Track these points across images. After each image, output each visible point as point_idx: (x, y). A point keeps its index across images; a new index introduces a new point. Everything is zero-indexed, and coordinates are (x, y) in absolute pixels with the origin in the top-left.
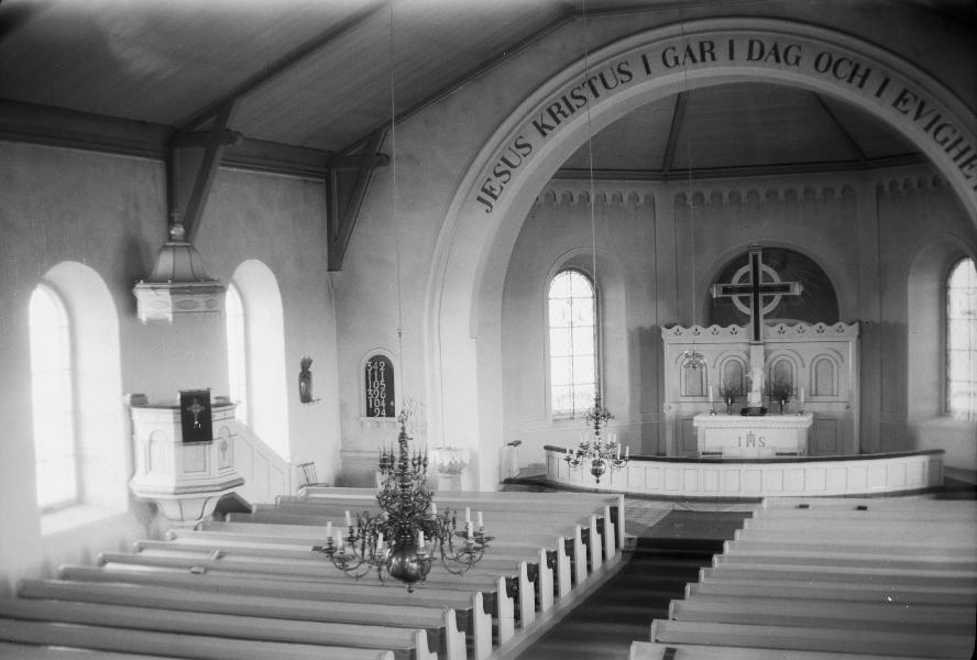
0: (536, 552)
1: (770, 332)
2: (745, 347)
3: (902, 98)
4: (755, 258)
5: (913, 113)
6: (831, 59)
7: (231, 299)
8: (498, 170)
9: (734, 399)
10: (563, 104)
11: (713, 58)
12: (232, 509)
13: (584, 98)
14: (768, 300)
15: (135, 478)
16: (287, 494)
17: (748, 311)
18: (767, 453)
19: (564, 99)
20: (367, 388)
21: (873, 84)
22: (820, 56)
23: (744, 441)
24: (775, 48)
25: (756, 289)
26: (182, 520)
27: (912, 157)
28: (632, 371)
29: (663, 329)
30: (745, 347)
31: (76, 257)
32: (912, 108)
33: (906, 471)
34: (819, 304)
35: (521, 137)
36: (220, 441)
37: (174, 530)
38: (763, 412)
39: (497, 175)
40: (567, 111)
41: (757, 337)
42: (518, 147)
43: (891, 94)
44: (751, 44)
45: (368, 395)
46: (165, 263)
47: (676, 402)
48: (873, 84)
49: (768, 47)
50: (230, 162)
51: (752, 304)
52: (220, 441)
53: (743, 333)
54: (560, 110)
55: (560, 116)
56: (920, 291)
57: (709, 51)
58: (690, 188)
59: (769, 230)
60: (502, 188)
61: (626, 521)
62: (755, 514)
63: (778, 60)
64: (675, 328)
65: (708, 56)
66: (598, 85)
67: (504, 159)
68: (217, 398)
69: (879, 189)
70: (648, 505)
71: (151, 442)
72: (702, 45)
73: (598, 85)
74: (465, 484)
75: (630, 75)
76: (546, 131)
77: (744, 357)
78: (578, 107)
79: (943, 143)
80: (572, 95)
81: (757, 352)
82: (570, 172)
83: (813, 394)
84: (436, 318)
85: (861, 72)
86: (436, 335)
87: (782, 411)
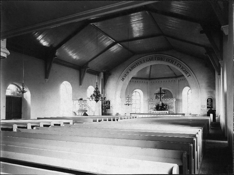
24: (161, 58)
31: (69, 81)
49: (160, 58)
66: (138, 64)
73: (138, 64)
82: (133, 78)
85: (173, 61)
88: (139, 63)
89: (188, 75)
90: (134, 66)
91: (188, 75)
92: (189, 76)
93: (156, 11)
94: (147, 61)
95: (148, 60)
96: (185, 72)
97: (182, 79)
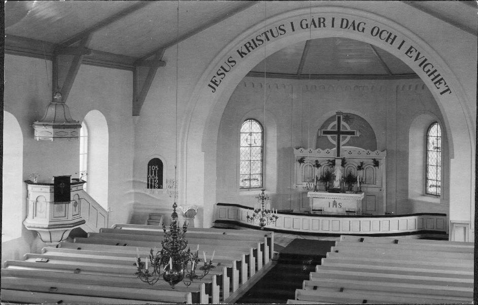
0: (231, 262)
4: (339, 118)
5: (414, 58)
6: (379, 30)
7: (83, 131)
12: (78, 236)
13: (262, 41)
15: (27, 220)
16: (106, 227)
17: (335, 143)
18: (340, 211)
19: (253, 40)
20: (148, 174)
22: (374, 28)
23: (331, 205)
24: (354, 23)
25: (339, 133)
26: (51, 242)
27: (414, 75)
29: (295, 150)
33: (408, 223)
35: (231, 57)
36: (74, 201)
37: (46, 248)
39: (219, 75)
40: (254, 46)
42: (230, 62)
44: (343, 20)
45: (148, 178)
46: (51, 112)
50: (85, 62)
51: (341, 127)
52: (74, 201)
55: (250, 48)
56: (415, 137)
57: (323, 22)
60: (220, 81)
61: (274, 244)
62: (336, 243)
63: (354, 29)
64: (301, 149)
65: (322, 24)
66: (269, 35)
67: (222, 67)
68: (73, 179)
70: (285, 236)
71: (37, 201)
72: (319, 19)
73: (269, 35)
74: (196, 223)
76: (243, 55)
78: (259, 45)
79: (427, 72)
80: (257, 39)
82: (254, 73)
84: (185, 140)
85: (392, 37)
86: (185, 160)
87: (350, 190)
89: (443, 88)
91: (443, 88)
94: (304, 26)
96: (432, 77)
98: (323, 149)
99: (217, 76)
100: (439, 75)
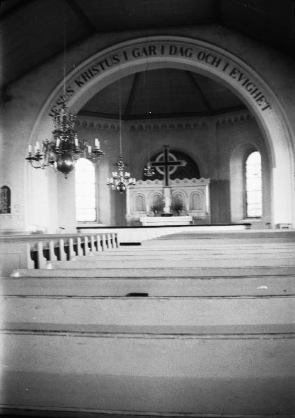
1: (173, 183)
2: (161, 189)
3: (233, 72)
5: (237, 79)
6: (205, 54)
8: (59, 102)
9: (158, 209)
10: (88, 73)
11: (155, 53)
14: (171, 169)
19: (89, 71)
21: (222, 66)
28: (111, 203)
30: (161, 189)
32: (237, 76)
34: (191, 171)
38: (170, 215)
39: (59, 104)
41: (167, 184)
43: (229, 70)
44: (171, 47)
47: (131, 213)
48: (222, 66)
51: (168, 158)
53: (161, 183)
54: (88, 75)
55: (87, 78)
56: (235, 165)
58: (136, 124)
59: (171, 141)
66: (104, 64)
69: (218, 124)
72: (150, 47)
73: (104, 64)
75: (72, 91)
77: (161, 193)
81: (167, 191)
82: (84, 112)
83: (192, 209)
85: (217, 60)
88: (110, 63)
90: (93, 72)
92: (266, 108)
93: (135, 85)
94: (136, 55)
95: (139, 54)
97: (242, 119)
98: (190, 179)
99: (56, 105)
100: (260, 93)
